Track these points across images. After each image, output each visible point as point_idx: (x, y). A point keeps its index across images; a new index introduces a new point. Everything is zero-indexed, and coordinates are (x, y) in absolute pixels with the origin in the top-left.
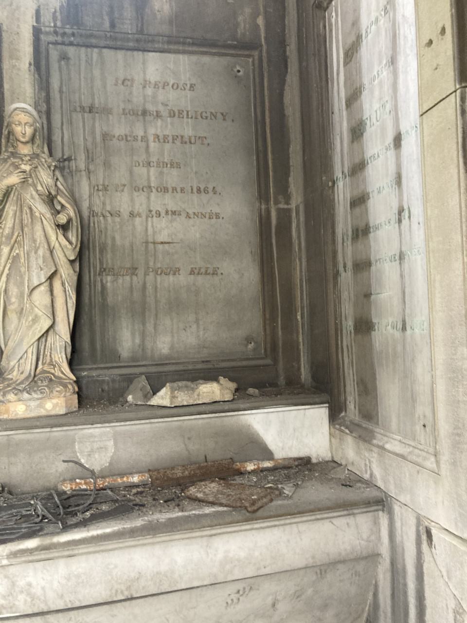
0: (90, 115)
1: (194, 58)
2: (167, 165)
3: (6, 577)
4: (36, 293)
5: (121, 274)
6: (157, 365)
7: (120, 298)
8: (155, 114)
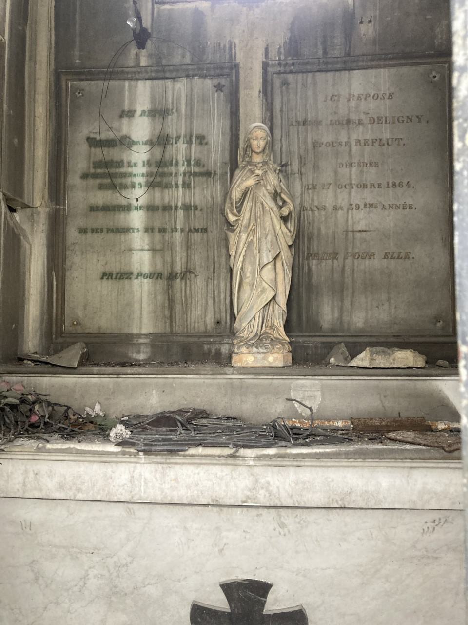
0: (304, 127)
1: (393, 71)
2: (366, 164)
3: (252, 474)
4: (265, 270)
5: (325, 258)
6: (352, 336)
7: (322, 279)
8: (357, 122)
